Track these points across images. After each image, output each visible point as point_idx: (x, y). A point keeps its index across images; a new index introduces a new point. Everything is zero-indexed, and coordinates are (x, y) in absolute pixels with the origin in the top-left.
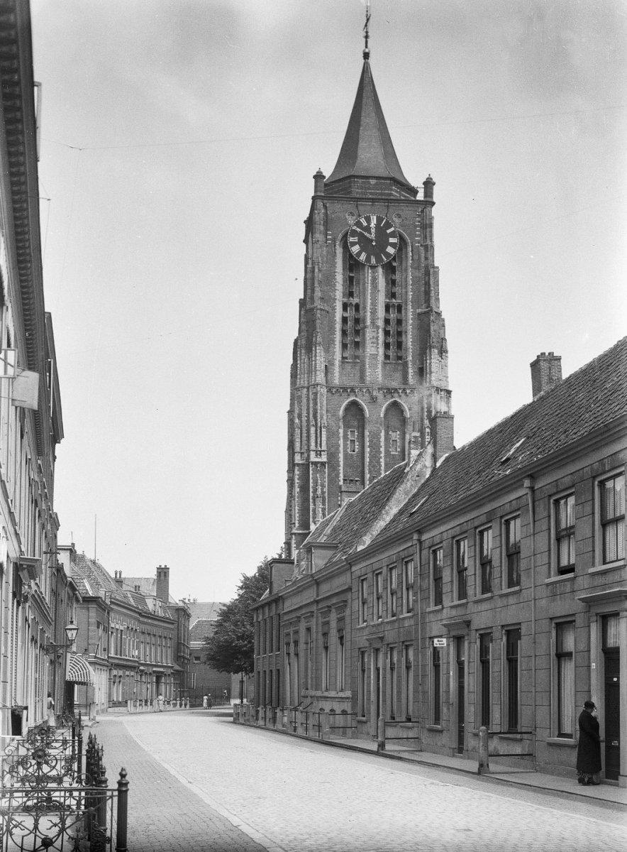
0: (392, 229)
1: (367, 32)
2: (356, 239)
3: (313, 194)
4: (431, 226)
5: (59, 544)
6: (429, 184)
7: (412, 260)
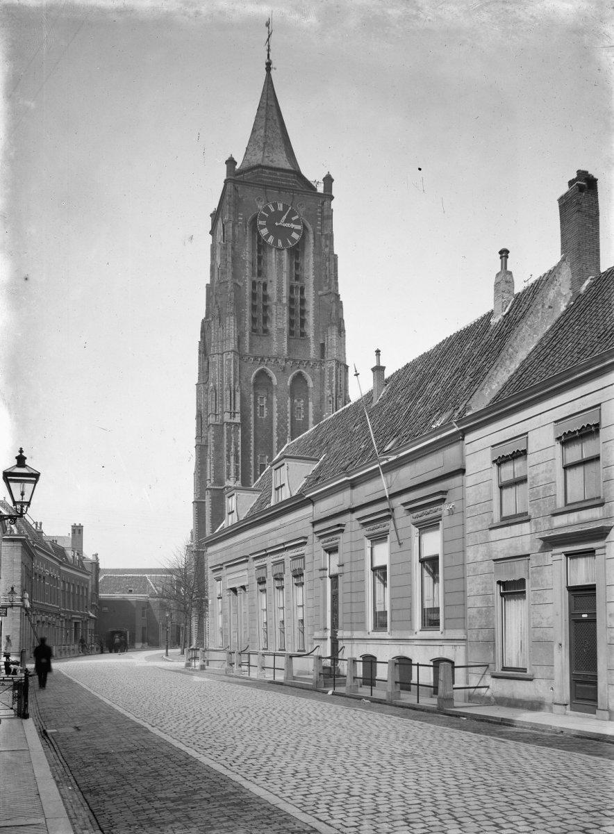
0: (297, 217)
1: (269, 46)
3: (225, 178)
4: (330, 217)
6: (328, 180)
7: (314, 246)
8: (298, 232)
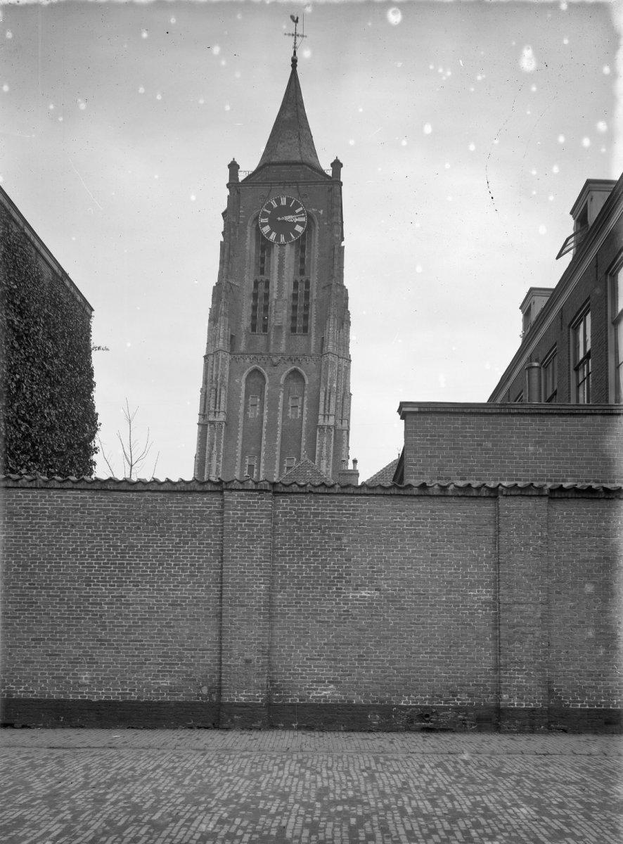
0: (301, 209)
2: (266, 220)
6: (337, 165)
8: (301, 224)
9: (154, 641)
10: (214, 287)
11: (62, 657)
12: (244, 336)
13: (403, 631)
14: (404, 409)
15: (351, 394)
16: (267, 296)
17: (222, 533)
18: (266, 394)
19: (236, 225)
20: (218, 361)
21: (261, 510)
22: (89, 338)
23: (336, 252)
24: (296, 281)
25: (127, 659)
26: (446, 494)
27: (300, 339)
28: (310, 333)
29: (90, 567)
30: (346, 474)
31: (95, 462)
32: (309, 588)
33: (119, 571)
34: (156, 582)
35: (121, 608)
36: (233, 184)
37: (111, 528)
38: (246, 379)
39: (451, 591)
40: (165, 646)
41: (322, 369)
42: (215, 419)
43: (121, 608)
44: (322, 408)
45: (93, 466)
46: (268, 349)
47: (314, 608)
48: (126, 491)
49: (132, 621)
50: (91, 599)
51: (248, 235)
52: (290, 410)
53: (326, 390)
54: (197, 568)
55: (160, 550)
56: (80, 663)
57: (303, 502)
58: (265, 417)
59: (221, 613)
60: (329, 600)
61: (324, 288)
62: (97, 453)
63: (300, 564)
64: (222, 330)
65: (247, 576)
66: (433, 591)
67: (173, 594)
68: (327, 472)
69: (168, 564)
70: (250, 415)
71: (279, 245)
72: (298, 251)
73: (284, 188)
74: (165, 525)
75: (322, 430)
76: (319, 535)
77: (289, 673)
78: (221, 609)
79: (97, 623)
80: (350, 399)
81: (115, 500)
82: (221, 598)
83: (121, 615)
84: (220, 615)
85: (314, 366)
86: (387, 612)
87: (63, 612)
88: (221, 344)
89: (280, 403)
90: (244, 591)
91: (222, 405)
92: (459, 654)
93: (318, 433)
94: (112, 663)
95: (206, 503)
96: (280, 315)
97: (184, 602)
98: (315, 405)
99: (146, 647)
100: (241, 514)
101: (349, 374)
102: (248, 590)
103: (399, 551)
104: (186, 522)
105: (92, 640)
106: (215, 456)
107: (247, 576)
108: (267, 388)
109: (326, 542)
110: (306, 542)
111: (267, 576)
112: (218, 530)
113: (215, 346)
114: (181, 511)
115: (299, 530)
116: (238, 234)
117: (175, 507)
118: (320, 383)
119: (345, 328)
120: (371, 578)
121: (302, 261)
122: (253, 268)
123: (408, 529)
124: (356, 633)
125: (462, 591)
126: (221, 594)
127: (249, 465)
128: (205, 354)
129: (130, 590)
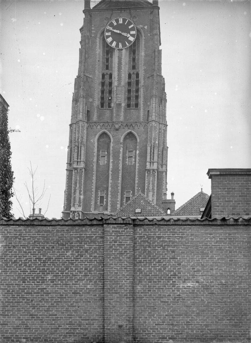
0: (132, 26)
2: (109, 34)
5: (59, 216)
9: (64, 315)
10: (76, 79)
11: (9, 325)
12: (96, 111)
13: (213, 307)
14: (211, 173)
15: (168, 148)
16: (111, 84)
17: (103, 250)
18: (111, 149)
19: (89, 37)
20: (79, 128)
21: (126, 236)
22: (6, 123)
23: (156, 53)
24: (130, 73)
25: (48, 326)
26: (237, 224)
27: (133, 112)
28: (140, 108)
29: (25, 271)
30: (167, 203)
31: (11, 202)
32: (156, 282)
33: (42, 273)
34: (64, 280)
35: (43, 295)
36: (87, 11)
37: (37, 248)
38: (98, 140)
39: (242, 282)
40: (70, 318)
41: (149, 131)
42: (78, 167)
43: (43, 295)
44: (148, 157)
45: (11, 205)
46: (112, 119)
47: (159, 294)
48: (45, 225)
49: (50, 303)
50: (26, 290)
51: (98, 44)
52: (127, 159)
53: (151, 145)
54: (89, 271)
55: (66, 260)
56: (20, 329)
57: (151, 230)
58: (111, 164)
59: (104, 298)
60: (168, 289)
61: (149, 77)
62: (12, 196)
63: (150, 267)
64: (81, 106)
65: (119, 275)
66: (230, 282)
67: (75, 287)
68: (153, 200)
69: (71, 269)
70: (101, 163)
71: (118, 50)
72: (131, 53)
73: (121, 12)
74: (69, 245)
75: (149, 172)
76: (161, 250)
77: (145, 334)
78: (104, 295)
79: (29, 305)
80: (167, 151)
81: (39, 231)
82: (103, 289)
83: (44, 300)
84: (103, 299)
85: (143, 129)
86: (203, 296)
87: (9, 298)
88: (81, 116)
89: (121, 155)
90: (117, 284)
91: (82, 157)
92: (247, 320)
93: (146, 174)
94: (39, 329)
95: (93, 232)
96: (119, 97)
97: (82, 291)
98: (143, 155)
99: (59, 319)
100: (115, 238)
101: (166, 133)
102: (119, 284)
103: (210, 258)
104: (82, 243)
105: (27, 315)
106: (78, 191)
107: (119, 275)
108: (112, 145)
109: (165, 254)
110: (153, 254)
111: (131, 275)
112: (101, 248)
113: (77, 118)
114: (78, 237)
115: (149, 247)
116: (90, 44)
117: (75, 234)
118: (147, 142)
119: (163, 104)
120: (193, 275)
121: (134, 60)
122: (101, 65)
123: (215, 245)
124: (185, 308)
125: (248, 282)
126: (104, 286)
127: (100, 197)
128: (70, 123)
129: (49, 284)
